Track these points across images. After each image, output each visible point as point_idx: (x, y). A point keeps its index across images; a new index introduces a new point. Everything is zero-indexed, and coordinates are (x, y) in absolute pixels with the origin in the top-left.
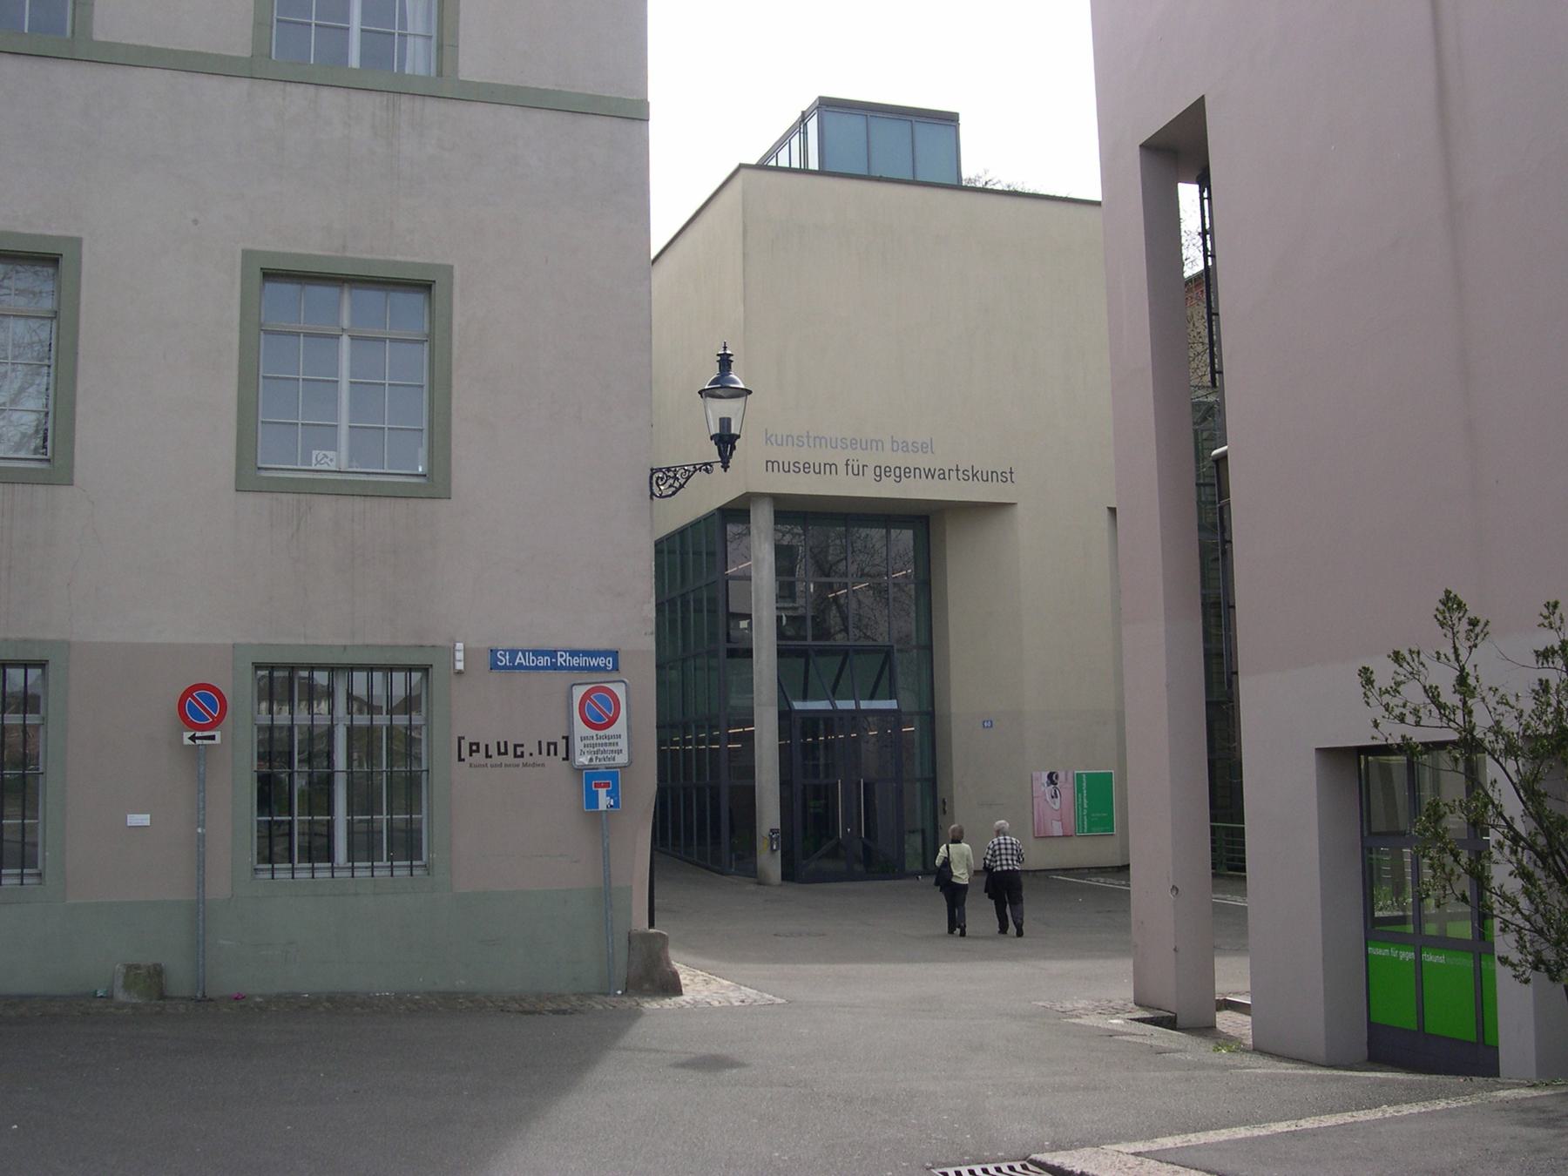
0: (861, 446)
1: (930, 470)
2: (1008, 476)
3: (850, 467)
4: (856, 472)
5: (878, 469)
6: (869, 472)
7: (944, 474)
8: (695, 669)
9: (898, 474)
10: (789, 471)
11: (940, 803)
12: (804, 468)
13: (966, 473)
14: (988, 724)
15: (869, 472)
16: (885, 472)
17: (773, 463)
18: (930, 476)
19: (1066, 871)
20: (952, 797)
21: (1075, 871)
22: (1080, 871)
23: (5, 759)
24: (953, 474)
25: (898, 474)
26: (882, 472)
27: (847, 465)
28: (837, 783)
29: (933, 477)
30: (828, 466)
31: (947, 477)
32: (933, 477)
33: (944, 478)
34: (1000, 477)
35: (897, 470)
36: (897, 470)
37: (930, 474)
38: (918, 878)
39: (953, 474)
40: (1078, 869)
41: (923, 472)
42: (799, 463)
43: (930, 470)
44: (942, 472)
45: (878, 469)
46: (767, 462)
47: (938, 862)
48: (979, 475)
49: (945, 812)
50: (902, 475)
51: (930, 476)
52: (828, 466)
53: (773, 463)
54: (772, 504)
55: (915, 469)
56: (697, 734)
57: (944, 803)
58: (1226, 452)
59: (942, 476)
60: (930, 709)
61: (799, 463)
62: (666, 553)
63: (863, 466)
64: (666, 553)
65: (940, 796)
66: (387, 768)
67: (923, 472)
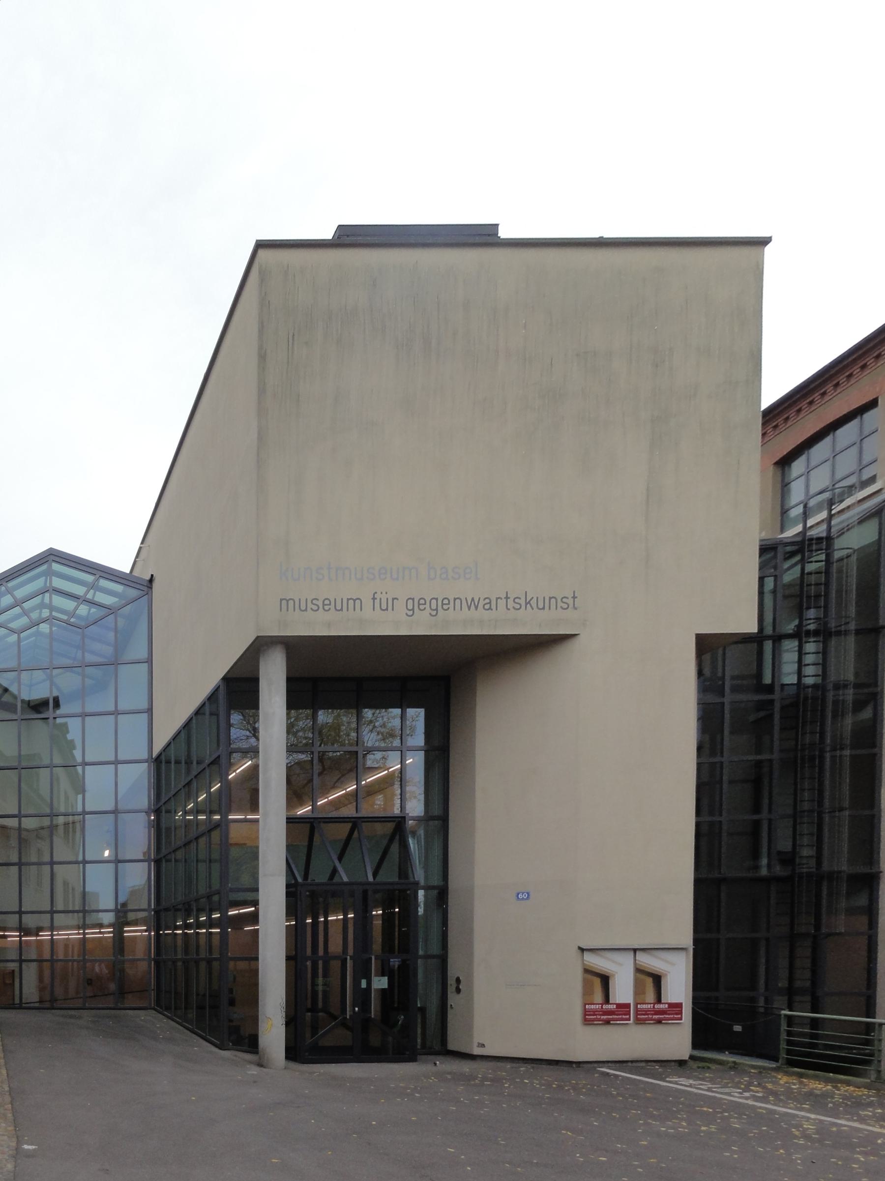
0: (391, 576)
1: (473, 599)
2: (570, 601)
3: (377, 602)
4: (384, 607)
5: (410, 602)
6: (400, 606)
7: (490, 603)
8: (197, 861)
9: (434, 607)
10: (306, 610)
11: (451, 982)
12: (324, 605)
13: (517, 600)
14: (523, 896)
15: (400, 606)
16: (419, 604)
17: (287, 601)
18: (473, 607)
19: (620, 1064)
20: (470, 976)
21: (630, 1064)
22: (634, 1064)
23: (195, 968)
24: (502, 603)
25: (434, 607)
26: (416, 605)
27: (374, 599)
28: (371, 958)
29: (476, 608)
30: (351, 602)
31: (494, 607)
32: (476, 608)
33: (490, 609)
34: (560, 604)
35: (434, 602)
36: (434, 602)
37: (473, 604)
38: (435, 1064)
39: (502, 603)
40: (632, 1062)
41: (464, 602)
42: (317, 600)
43: (473, 599)
44: (487, 601)
45: (410, 602)
46: (281, 600)
47: (715, 1130)
48: (534, 602)
49: (458, 991)
50: (440, 608)
51: (473, 607)
52: (351, 602)
53: (287, 601)
54: (285, 651)
55: (455, 599)
56: (197, 918)
57: (458, 981)
58: (258, 929)
59: (487, 607)
60: (441, 883)
61: (317, 600)
62: (173, 763)
63: (393, 599)
64: (173, 763)
65: (453, 972)
66: (79, 956)
67: (464, 602)
